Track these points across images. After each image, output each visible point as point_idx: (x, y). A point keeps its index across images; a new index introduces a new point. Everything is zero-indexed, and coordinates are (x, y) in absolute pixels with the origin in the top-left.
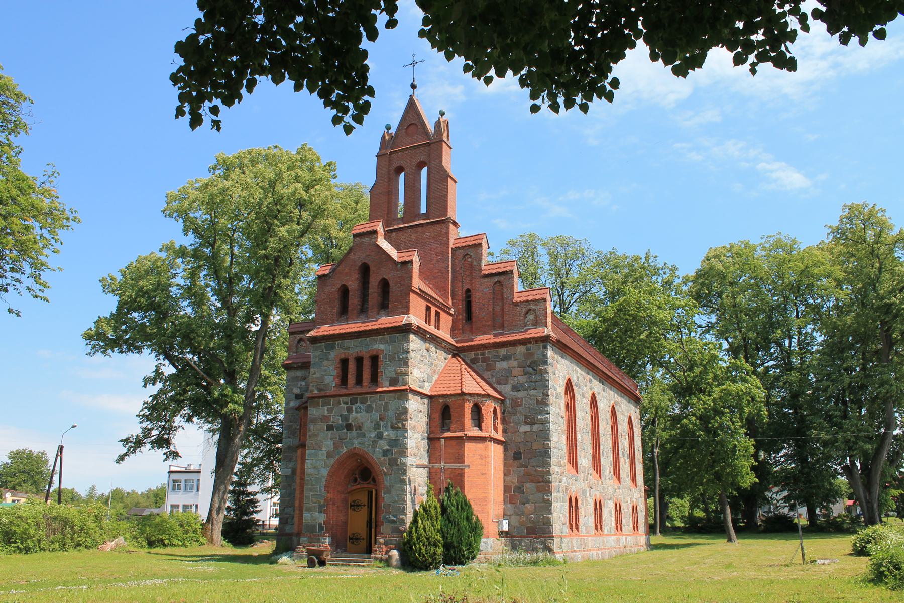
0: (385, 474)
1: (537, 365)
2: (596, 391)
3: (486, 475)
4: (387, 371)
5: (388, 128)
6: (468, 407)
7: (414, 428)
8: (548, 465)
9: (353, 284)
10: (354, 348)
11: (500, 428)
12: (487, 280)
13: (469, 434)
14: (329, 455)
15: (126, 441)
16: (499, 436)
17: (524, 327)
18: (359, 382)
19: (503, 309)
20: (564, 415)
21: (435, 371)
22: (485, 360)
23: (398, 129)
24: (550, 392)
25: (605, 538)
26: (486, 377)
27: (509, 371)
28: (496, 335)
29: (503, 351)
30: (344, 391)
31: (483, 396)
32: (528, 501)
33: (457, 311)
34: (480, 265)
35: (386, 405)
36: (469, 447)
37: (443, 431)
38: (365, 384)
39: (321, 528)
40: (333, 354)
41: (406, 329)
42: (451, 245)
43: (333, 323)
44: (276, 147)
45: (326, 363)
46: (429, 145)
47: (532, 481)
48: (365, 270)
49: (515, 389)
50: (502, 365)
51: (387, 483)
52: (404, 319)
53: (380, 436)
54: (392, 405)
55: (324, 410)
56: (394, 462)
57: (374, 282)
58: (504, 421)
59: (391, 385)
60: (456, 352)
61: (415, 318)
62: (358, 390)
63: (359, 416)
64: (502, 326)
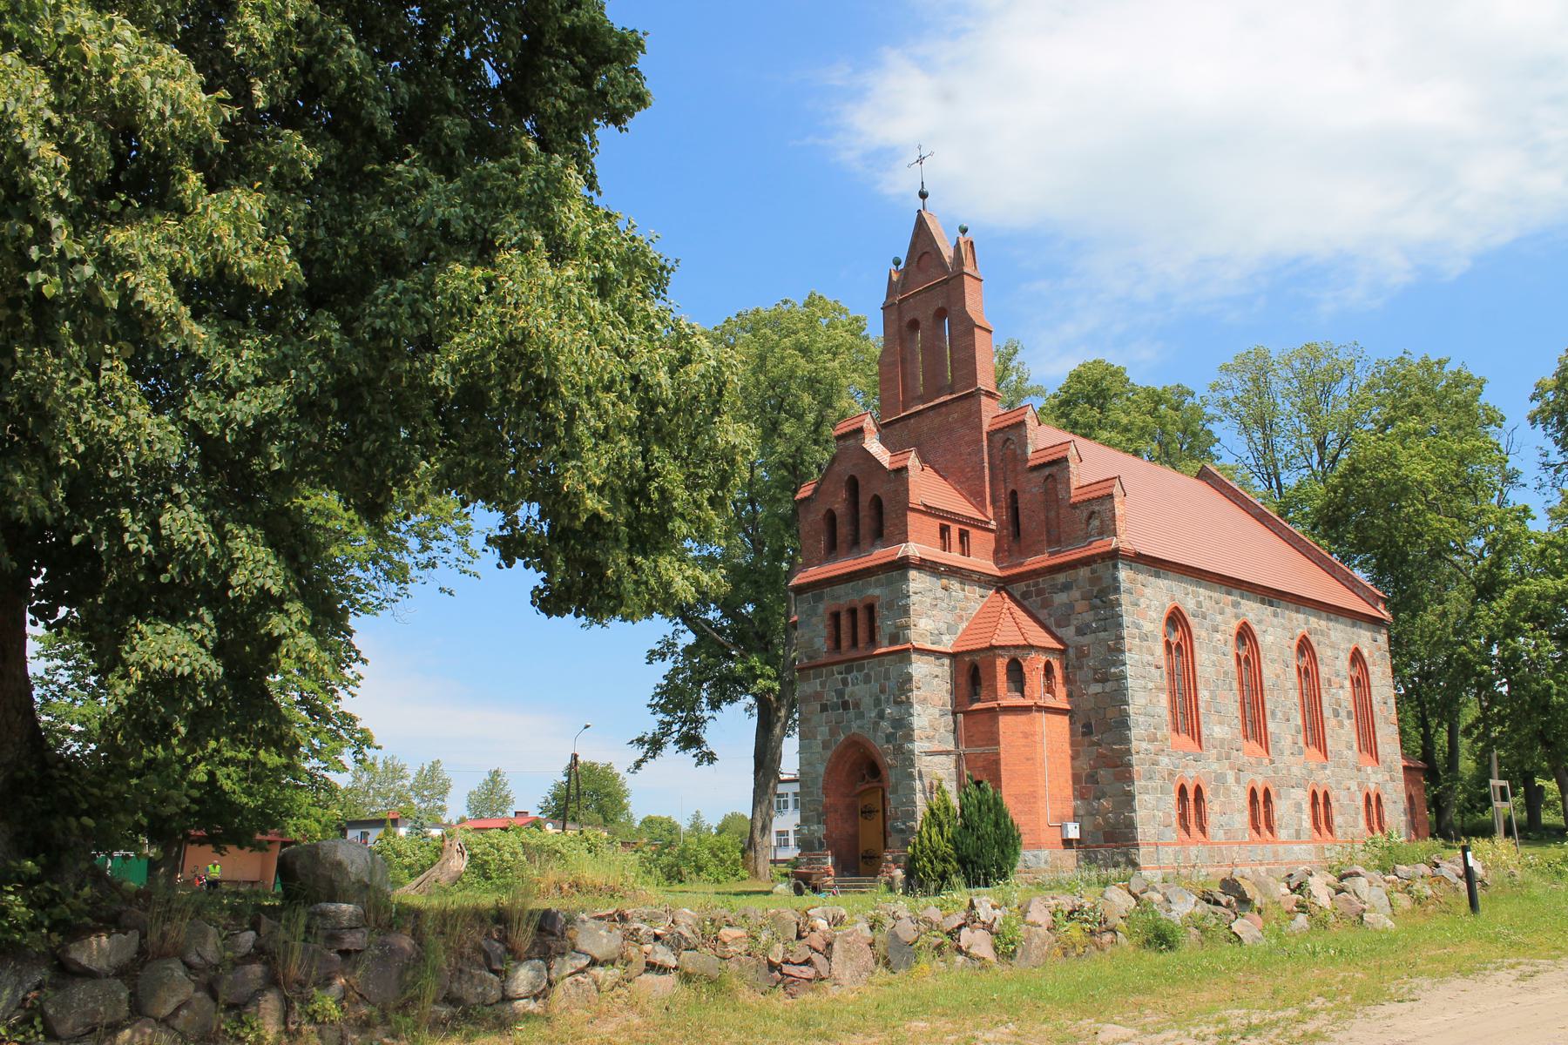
0: (890, 767)
1: (1107, 594)
2: (1251, 618)
3: (1039, 757)
4: (885, 625)
5: (897, 262)
6: (1001, 664)
7: (924, 701)
8: (1127, 741)
9: (840, 506)
10: (847, 596)
11: (1061, 690)
12: (1035, 474)
13: (1004, 703)
14: (825, 746)
15: (641, 741)
16: (1061, 701)
17: (1087, 538)
18: (854, 643)
19: (1058, 514)
20: (1163, 663)
21: (961, 617)
22: (1040, 593)
23: (908, 264)
24: (1125, 633)
25: (1281, 848)
26: (1041, 617)
27: (1070, 606)
28: (1051, 554)
29: (1061, 578)
30: (838, 657)
31: (1024, 647)
32: (1104, 795)
33: (1000, 523)
34: (1025, 453)
35: (887, 671)
36: (1005, 722)
37: (973, 702)
38: (861, 645)
39: (821, 844)
40: (821, 607)
41: (903, 565)
42: (986, 428)
43: (820, 564)
44: (785, 302)
45: (814, 620)
46: (946, 282)
47: (1108, 766)
48: (853, 485)
49: (1080, 631)
50: (1061, 598)
51: (892, 780)
52: (901, 550)
53: (881, 716)
54: (893, 672)
55: (816, 685)
56: (899, 750)
57: (864, 500)
58: (1067, 680)
59: (891, 644)
60: (1001, 585)
61: (912, 549)
62: (854, 654)
63: (858, 690)
64: (1058, 542)
